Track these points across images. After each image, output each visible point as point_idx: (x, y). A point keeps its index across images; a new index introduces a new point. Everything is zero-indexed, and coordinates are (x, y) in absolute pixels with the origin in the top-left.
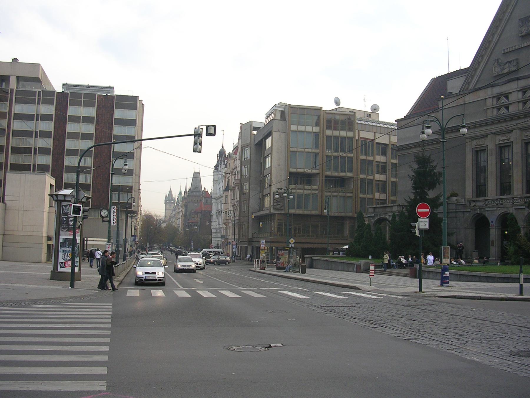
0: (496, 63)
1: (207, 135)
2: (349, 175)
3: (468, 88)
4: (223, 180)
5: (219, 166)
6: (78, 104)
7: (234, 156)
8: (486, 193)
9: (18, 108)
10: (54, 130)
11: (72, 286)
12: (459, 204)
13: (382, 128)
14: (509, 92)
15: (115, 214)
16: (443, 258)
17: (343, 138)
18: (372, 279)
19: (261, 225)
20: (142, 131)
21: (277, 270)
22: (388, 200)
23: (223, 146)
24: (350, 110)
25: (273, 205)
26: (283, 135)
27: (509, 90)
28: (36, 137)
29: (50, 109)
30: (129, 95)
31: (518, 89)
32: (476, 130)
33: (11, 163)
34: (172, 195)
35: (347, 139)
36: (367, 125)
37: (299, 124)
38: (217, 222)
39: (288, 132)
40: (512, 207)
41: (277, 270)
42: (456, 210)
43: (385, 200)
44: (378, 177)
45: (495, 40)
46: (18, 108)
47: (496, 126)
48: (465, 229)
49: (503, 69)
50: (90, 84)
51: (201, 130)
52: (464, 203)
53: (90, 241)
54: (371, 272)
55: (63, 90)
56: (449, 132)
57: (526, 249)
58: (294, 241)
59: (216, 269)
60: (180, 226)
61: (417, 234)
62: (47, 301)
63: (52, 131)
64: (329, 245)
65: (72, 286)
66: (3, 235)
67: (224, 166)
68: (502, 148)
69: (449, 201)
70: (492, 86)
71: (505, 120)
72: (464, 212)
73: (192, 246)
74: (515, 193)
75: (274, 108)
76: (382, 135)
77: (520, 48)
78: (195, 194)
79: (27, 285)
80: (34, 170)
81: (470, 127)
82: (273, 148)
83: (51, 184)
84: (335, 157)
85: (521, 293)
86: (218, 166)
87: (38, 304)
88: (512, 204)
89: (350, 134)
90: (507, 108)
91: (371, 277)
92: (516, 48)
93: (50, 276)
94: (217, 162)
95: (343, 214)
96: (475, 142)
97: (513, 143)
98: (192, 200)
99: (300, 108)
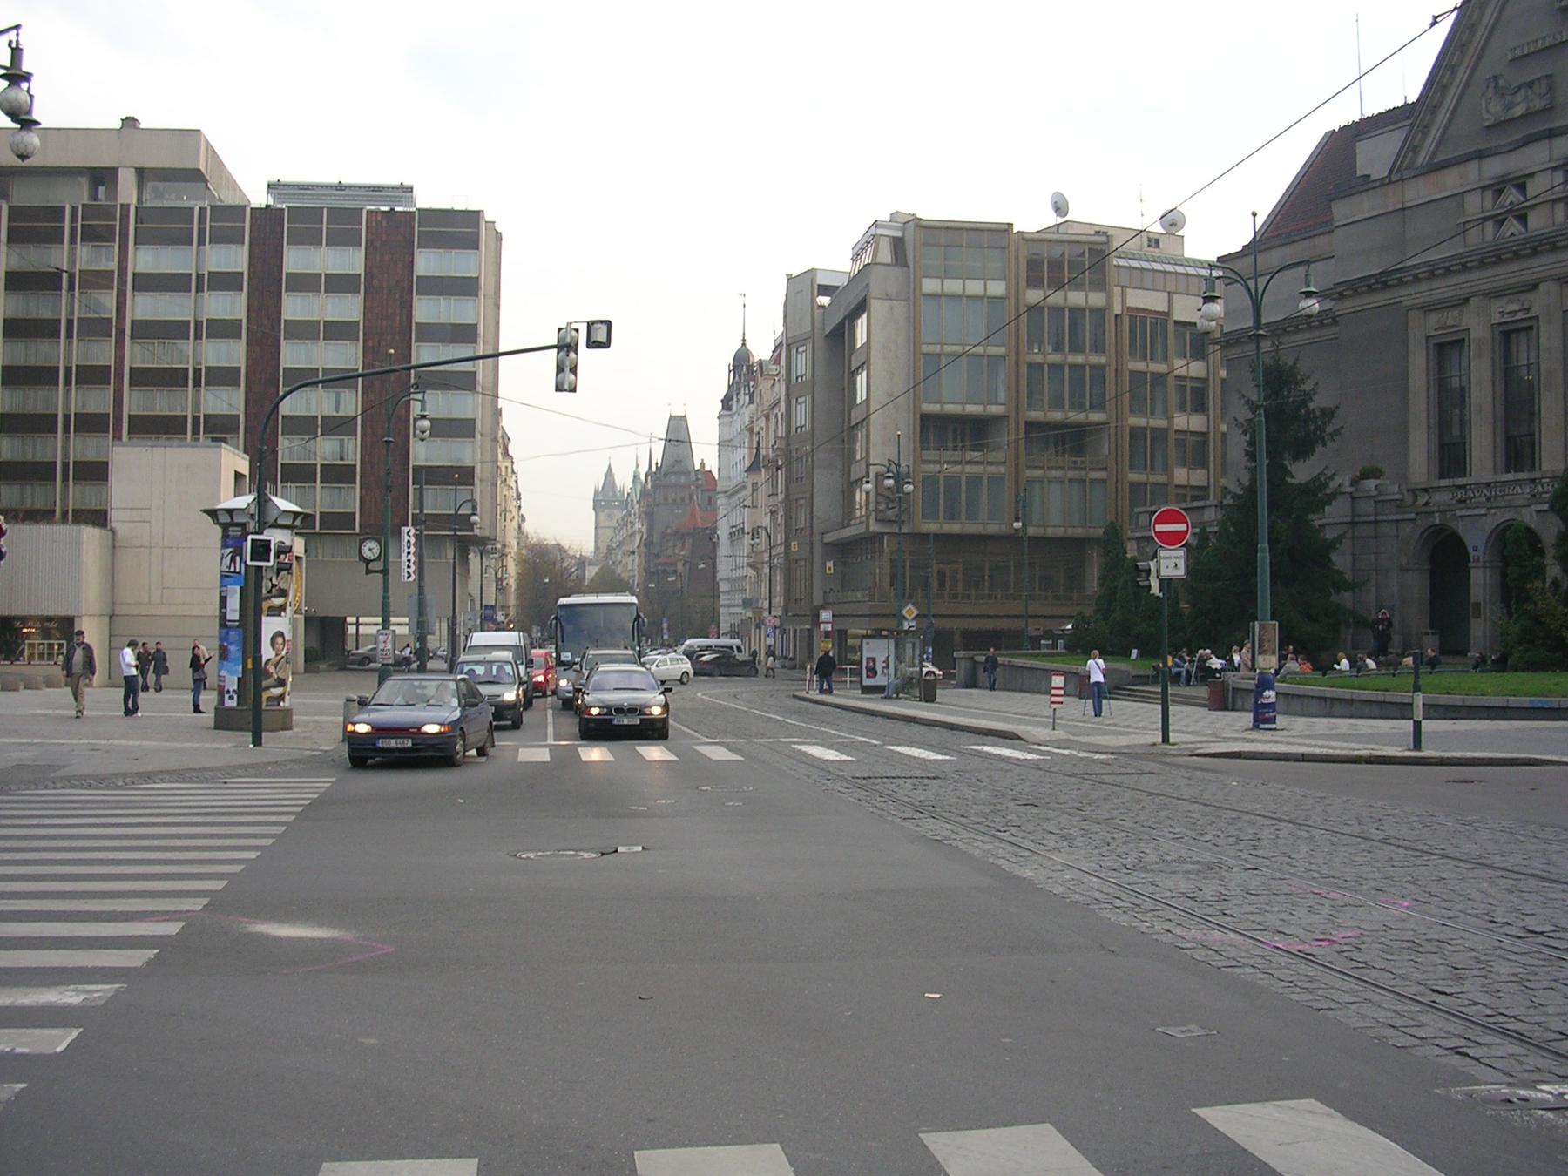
0: (1491, 89)
1: (589, 346)
2: (1096, 417)
3: (1412, 163)
4: (747, 440)
5: (735, 399)
6: (312, 239)
7: (774, 369)
8: (1465, 469)
9: (145, 260)
10: (248, 317)
11: (257, 741)
12: (1382, 498)
13: (1192, 280)
14: (1527, 172)
15: (412, 549)
16: (1259, 654)
17: (1077, 312)
18: (1057, 711)
19: (830, 569)
20: (499, 308)
21: (862, 693)
22: (1212, 488)
23: (744, 340)
24: (1098, 229)
25: (877, 511)
26: (900, 308)
27: (1530, 167)
28: (198, 336)
29: (236, 259)
30: (456, 208)
31: (1553, 165)
32: (1436, 284)
33: (132, 413)
34: (614, 483)
35: (1087, 314)
36: (1170, 272)
37: (947, 274)
38: (731, 563)
39: (913, 298)
40: (1529, 506)
41: (862, 693)
42: (1376, 515)
43: (1206, 489)
44: (1182, 421)
45: (1487, 20)
46: (145, 260)
47: (1489, 272)
48: (1402, 569)
49: (1510, 106)
50: (346, 181)
51: (574, 333)
52: (1396, 497)
53: (366, 624)
54: (1053, 692)
55: (271, 202)
56: (1489, 263)
57: (1552, 627)
58: (916, 612)
59: (699, 695)
60: (636, 573)
61: (1155, 589)
62: (179, 775)
63: (241, 320)
64: (1030, 620)
65: (257, 741)
66: (110, 617)
67: (747, 397)
68: (1507, 335)
69: (1357, 490)
70: (1480, 155)
71: (1516, 253)
72: (1398, 521)
73: (665, 631)
74: (1545, 466)
75: (872, 231)
76: (1268, 277)
77: (1556, 45)
78: (673, 479)
79: (144, 743)
80: (196, 431)
81: (1420, 276)
82: (872, 344)
83: (236, 473)
84: (1056, 368)
85: (1417, 744)
86: (732, 399)
87: (155, 783)
88: (1529, 496)
89: (1097, 299)
90: (1522, 219)
91: (1054, 706)
92: (1547, 44)
93: (213, 721)
94: (729, 387)
95: (1080, 532)
96: (1434, 318)
97: (1540, 319)
98: (666, 499)
99: (947, 228)
